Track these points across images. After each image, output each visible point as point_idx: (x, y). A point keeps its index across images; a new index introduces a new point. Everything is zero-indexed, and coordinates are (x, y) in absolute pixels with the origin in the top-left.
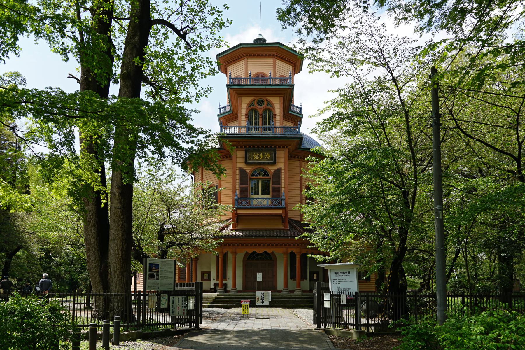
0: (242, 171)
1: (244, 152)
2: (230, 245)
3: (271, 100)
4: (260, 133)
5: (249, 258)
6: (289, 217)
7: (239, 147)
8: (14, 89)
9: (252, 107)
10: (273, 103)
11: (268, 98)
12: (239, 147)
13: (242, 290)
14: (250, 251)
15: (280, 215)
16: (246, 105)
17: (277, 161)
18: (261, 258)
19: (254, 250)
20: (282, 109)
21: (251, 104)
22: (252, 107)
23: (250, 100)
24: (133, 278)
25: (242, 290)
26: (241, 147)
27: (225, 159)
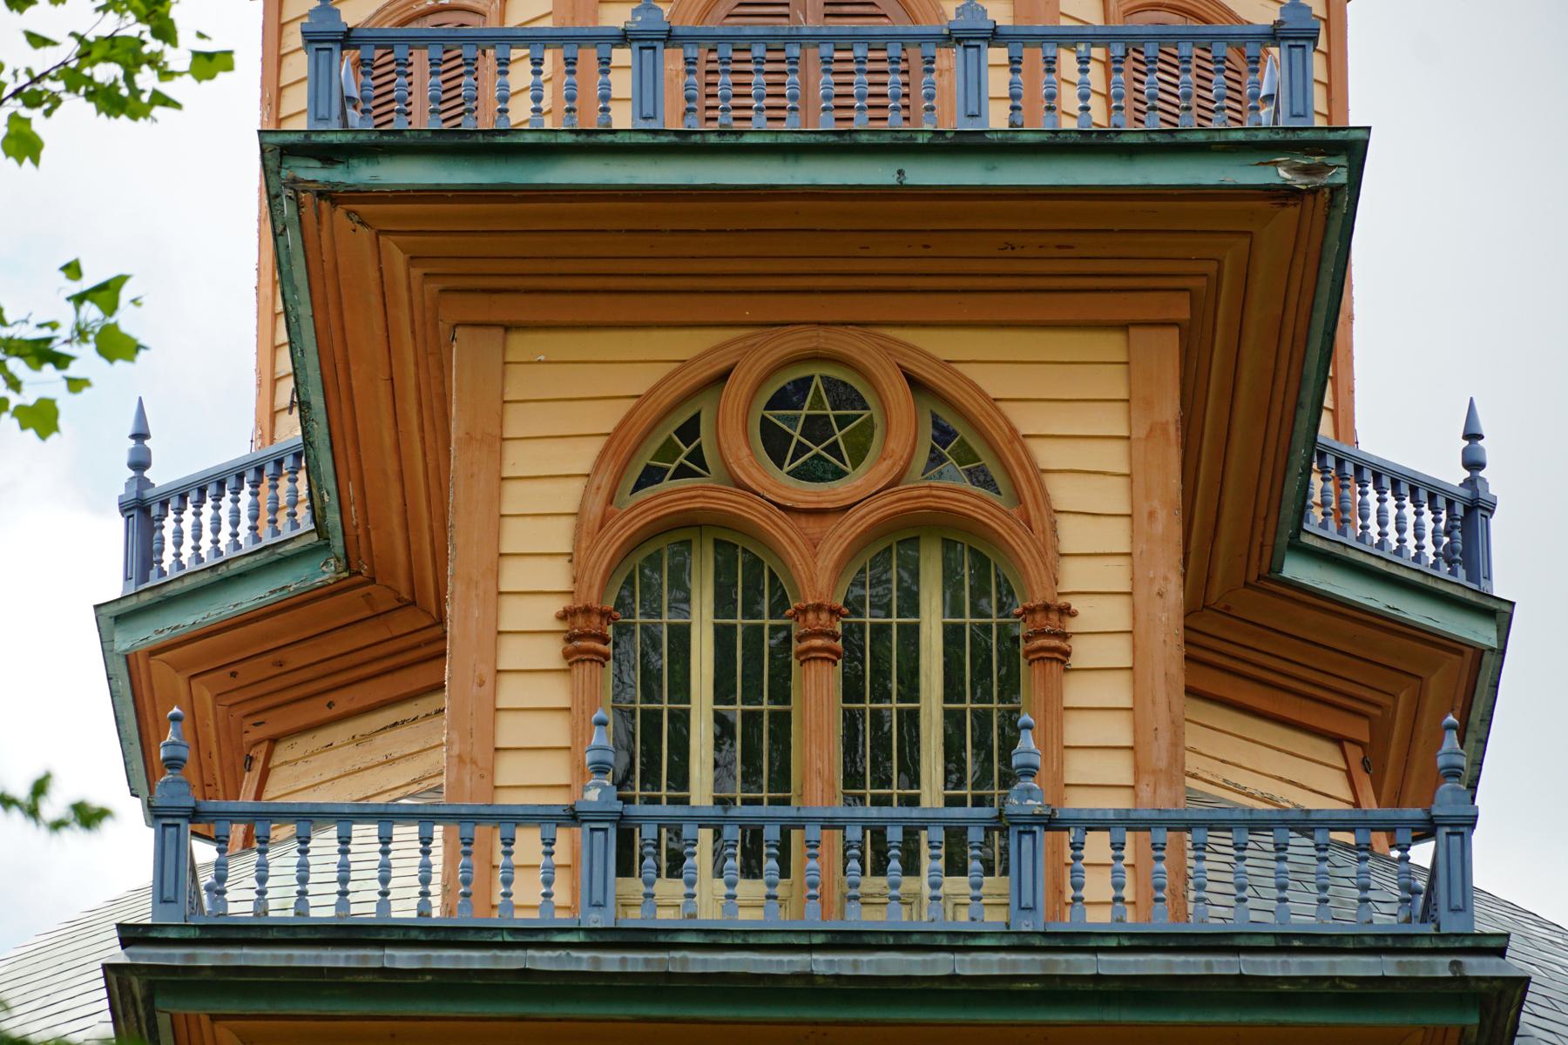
3: (994, 382)
16: (583, 457)
20: (1167, 526)
23: (641, 380)
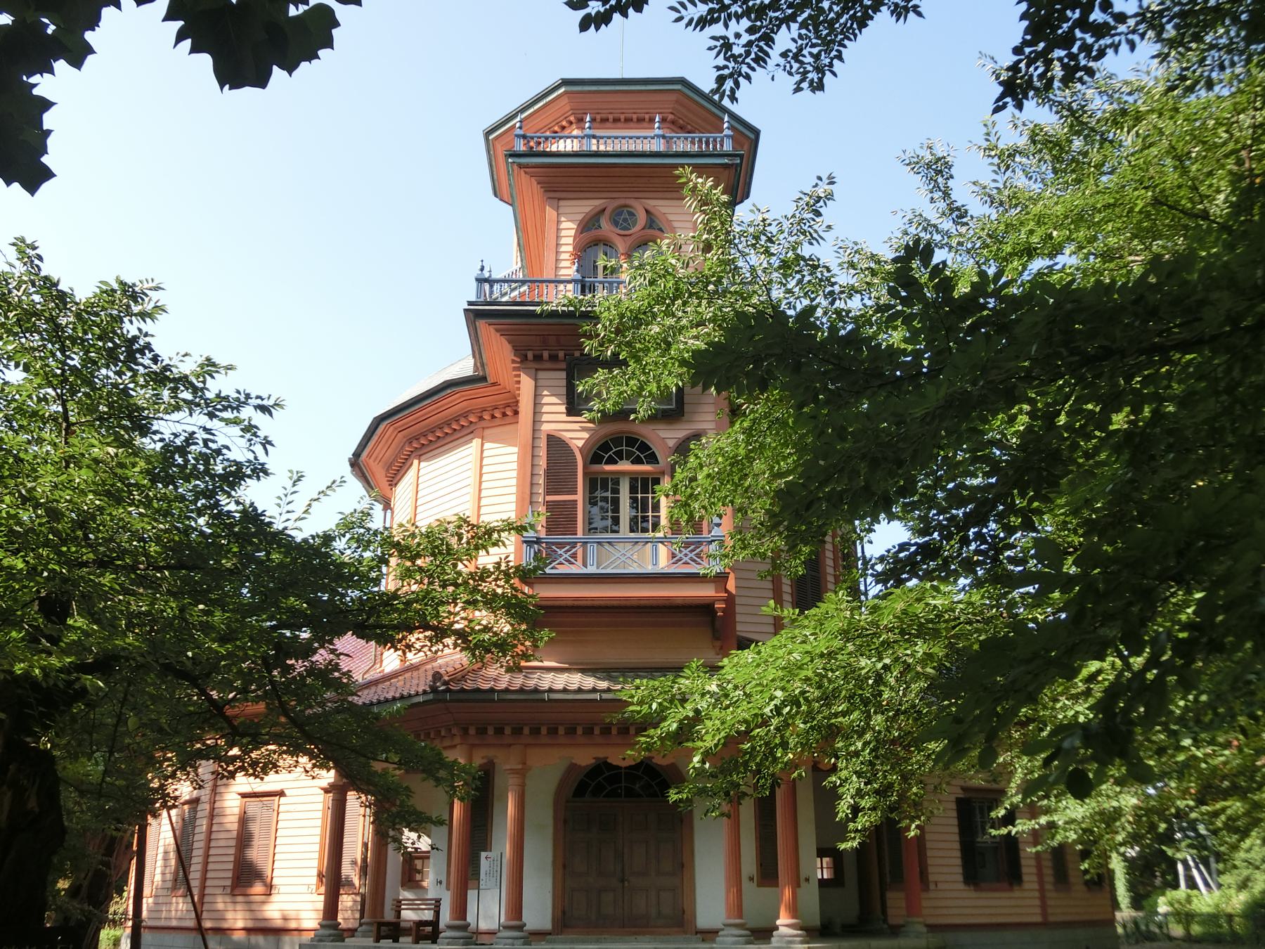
0: (555, 443)
1: (564, 375)
2: (499, 731)
3: (664, 210)
4: (663, 563)
5: (580, 791)
6: (739, 627)
7: (546, 354)
8: (437, 676)
9: (594, 233)
10: (671, 217)
11: (652, 202)
12: (546, 354)
13: (547, 925)
14: (585, 757)
15: (705, 608)
17: (686, 408)
18: (630, 793)
19: (601, 753)
21: (588, 225)
22: (594, 233)
23: (587, 209)
24: (134, 861)
25: (547, 925)
26: (554, 358)
27: (497, 422)
